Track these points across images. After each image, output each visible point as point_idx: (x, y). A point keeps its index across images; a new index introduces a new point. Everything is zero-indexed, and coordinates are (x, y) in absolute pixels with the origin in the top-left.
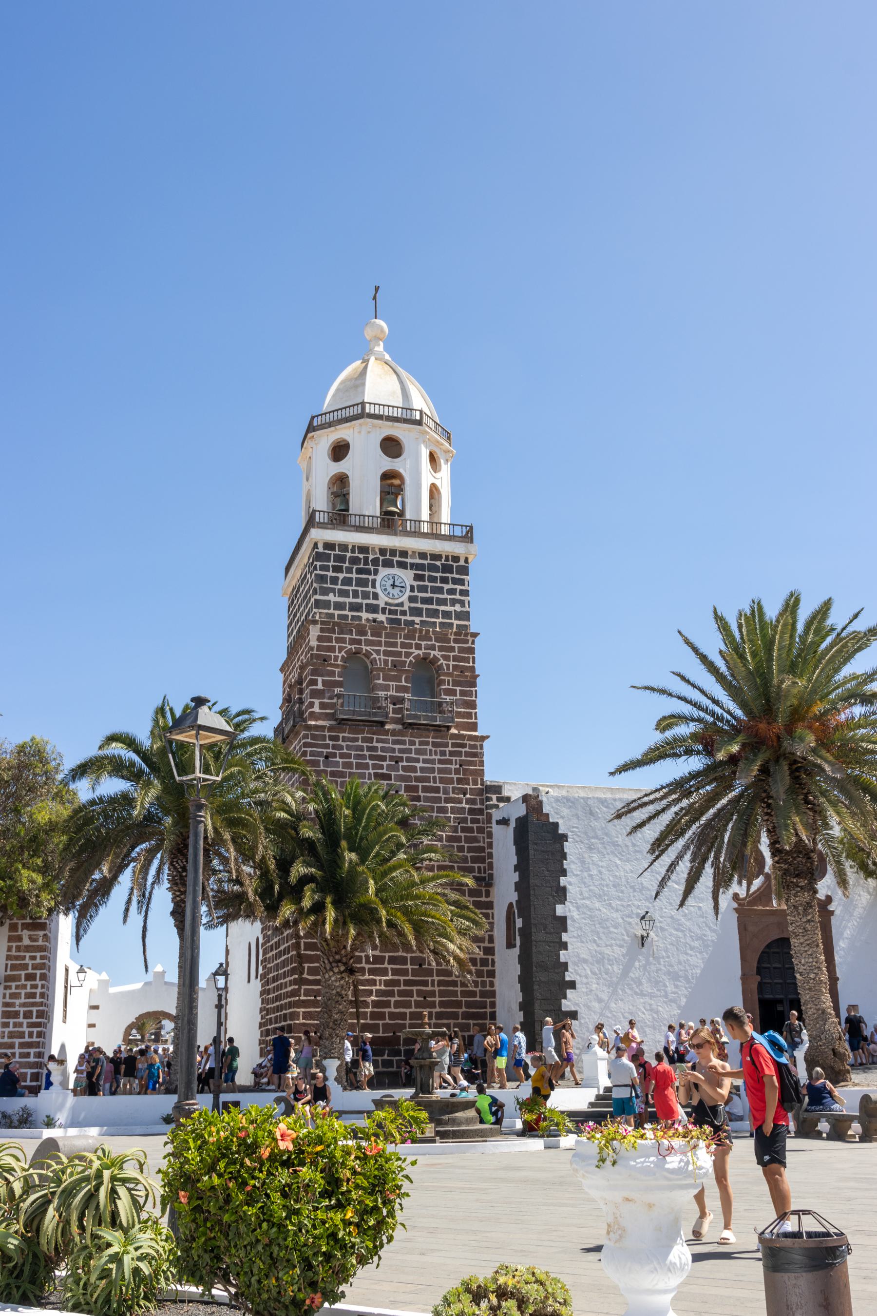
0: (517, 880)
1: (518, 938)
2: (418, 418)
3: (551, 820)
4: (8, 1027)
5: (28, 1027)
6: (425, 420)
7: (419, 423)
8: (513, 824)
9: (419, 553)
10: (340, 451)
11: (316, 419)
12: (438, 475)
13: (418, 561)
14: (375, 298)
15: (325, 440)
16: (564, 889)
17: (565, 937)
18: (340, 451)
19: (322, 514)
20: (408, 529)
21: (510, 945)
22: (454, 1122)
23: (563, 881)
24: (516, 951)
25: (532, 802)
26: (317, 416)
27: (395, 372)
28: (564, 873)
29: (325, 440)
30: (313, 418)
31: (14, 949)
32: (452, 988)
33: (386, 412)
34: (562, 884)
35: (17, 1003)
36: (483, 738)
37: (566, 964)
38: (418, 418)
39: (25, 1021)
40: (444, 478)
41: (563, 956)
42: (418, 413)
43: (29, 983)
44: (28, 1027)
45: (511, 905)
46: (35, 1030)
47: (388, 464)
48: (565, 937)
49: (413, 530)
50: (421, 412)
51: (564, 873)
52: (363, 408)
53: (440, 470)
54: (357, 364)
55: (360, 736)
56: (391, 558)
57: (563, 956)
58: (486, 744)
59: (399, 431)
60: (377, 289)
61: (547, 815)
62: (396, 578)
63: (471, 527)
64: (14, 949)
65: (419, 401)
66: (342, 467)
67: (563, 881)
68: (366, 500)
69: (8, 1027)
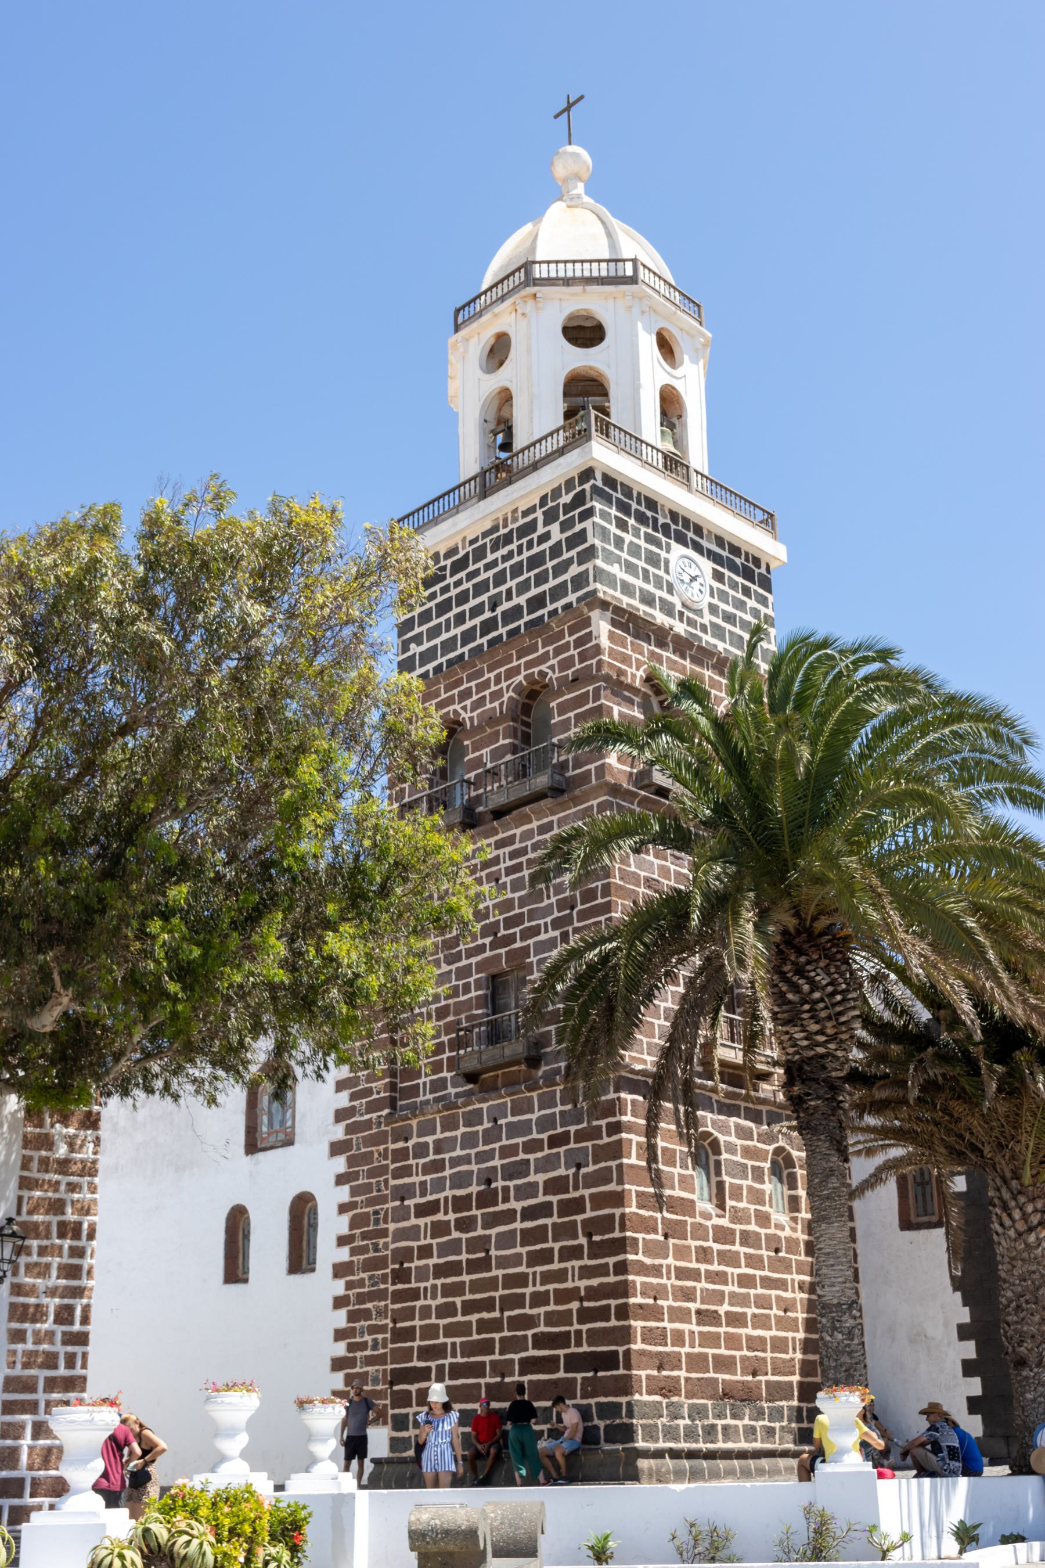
2: (629, 272)
4: (23, 1340)
5: (65, 1343)
6: (642, 273)
7: (633, 280)
9: (716, 537)
10: (498, 351)
13: (714, 548)
15: (479, 336)
18: (498, 351)
27: (603, 223)
29: (479, 336)
31: (35, 1165)
35: (42, 1289)
38: (629, 272)
39: (60, 1329)
40: (691, 381)
42: (629, 266)
43: (67, 1243)
44: (65, 1343)
46: (62, 1371)
50: (634, 261)
53: (682, 363)
54: (528, 227)
55: (475, 1337)
59: (597, 303)
64: (35, 1165)
65: (633, 246)
66: (504, 377)
69: (23, 1340)
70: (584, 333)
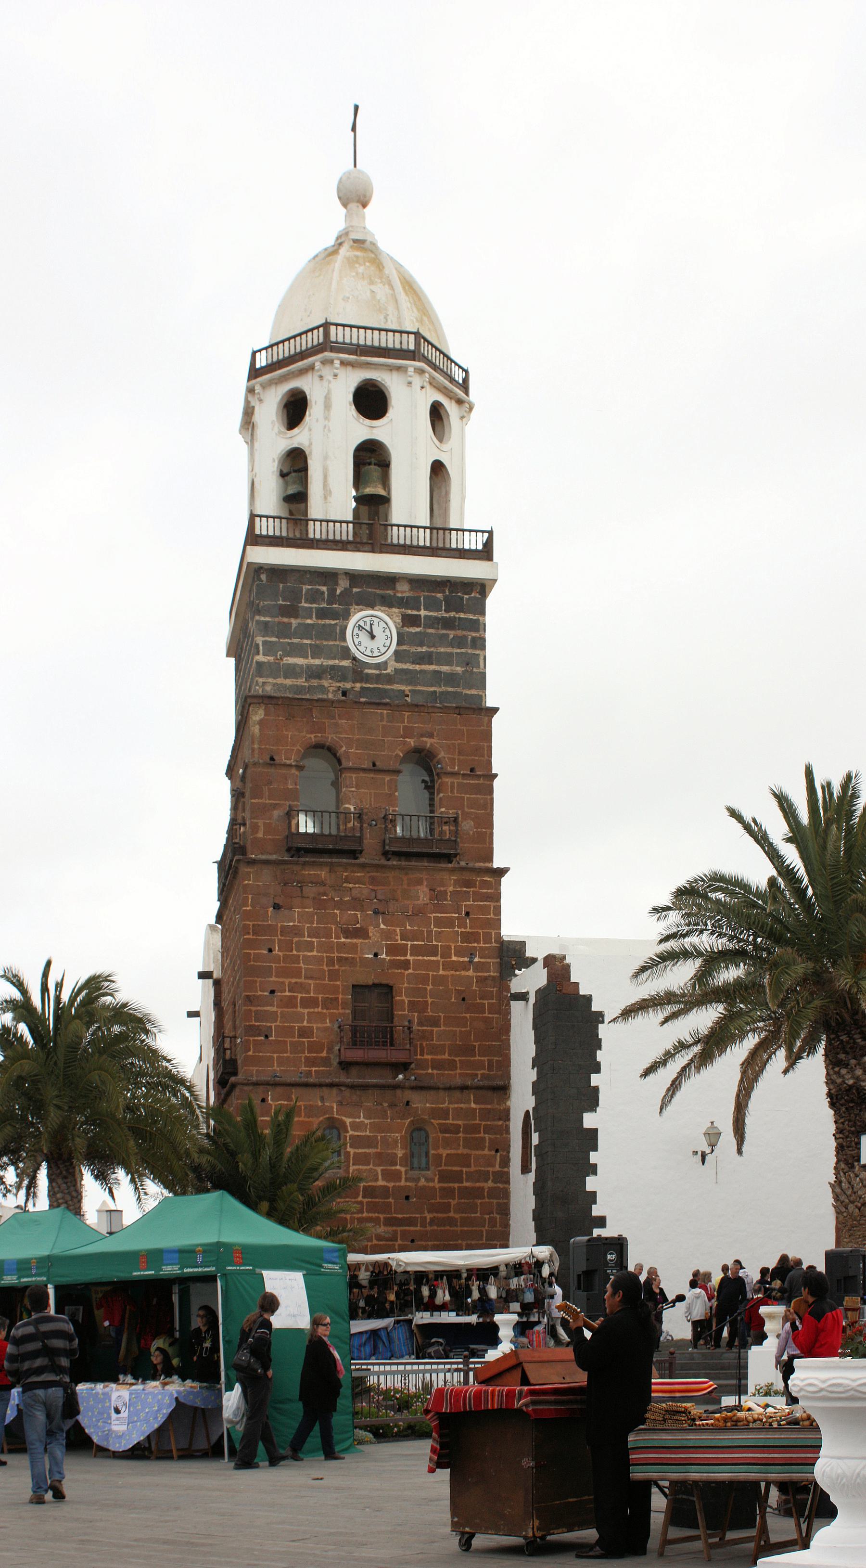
0: (535, 1078)
1: (534, 1159)
2: (412, 347)
3: (581, 993)
8: (532, 999)
11: (258, 355)
12: (444, 447)
14: (354, 129)
16: (596, 1089)
17: (594, 1157)
19: (317, 523)
20: (311, 536)
21: (525, 1169)
22: (556, 1402)
23: (595, 1080)
24: (532, 1176)
25: (557, 967)
26: (260, 351)
28: (597, 1069)
30: (254, 353)
32: (465, 1229)
33: (391, 341)
34: (593, 1084)
36: (502, 872)
37: (594, 1194)
38: (412, 347)
41: (591, 1183)
45: (528, 1112)
47: (364, 429)
48: (594, 1157)
49: (428, 544)
50: (417, 335)
51: (597, 1069)
52: (327, 334)
56: (376, 589)
57: (591, 1183)
58: (504, 880)
60: (356, 108)
61: (577, 984)
62: (361, 623)
63: (491, 533)
67: (595, 1080)
68: (333, 496)
70: (371, 401)
